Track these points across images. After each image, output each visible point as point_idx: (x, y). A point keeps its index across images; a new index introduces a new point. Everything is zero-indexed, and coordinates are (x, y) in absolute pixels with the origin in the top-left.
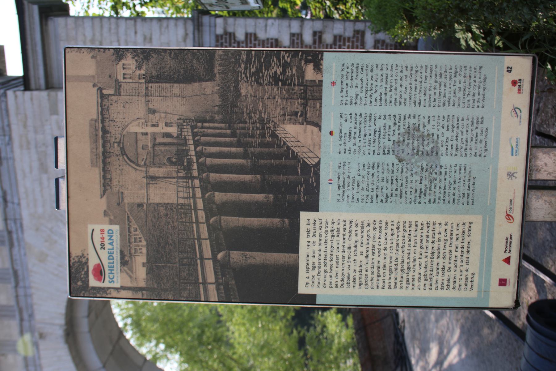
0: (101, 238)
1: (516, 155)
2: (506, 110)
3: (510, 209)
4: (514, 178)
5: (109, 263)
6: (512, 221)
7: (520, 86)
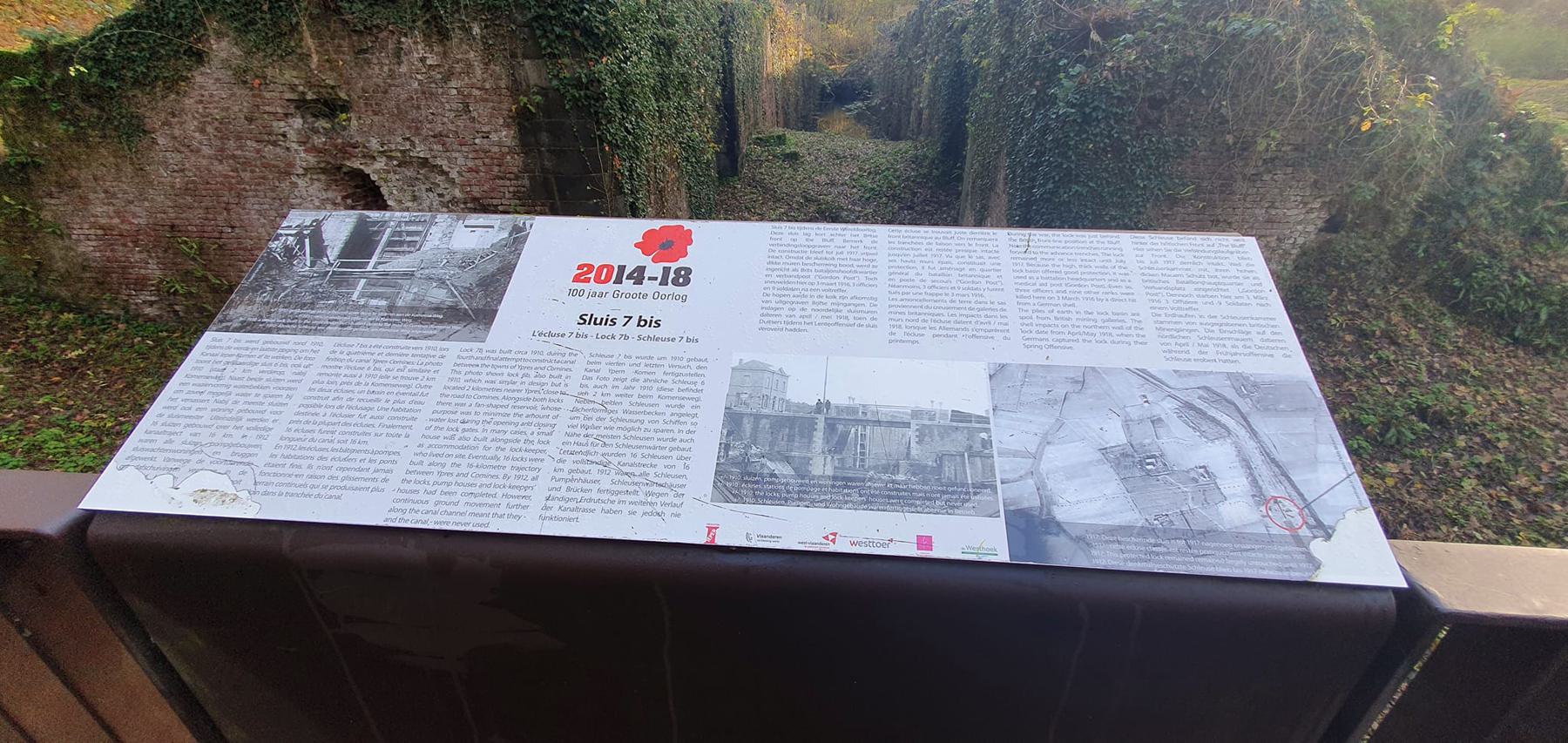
7: (638, 275)
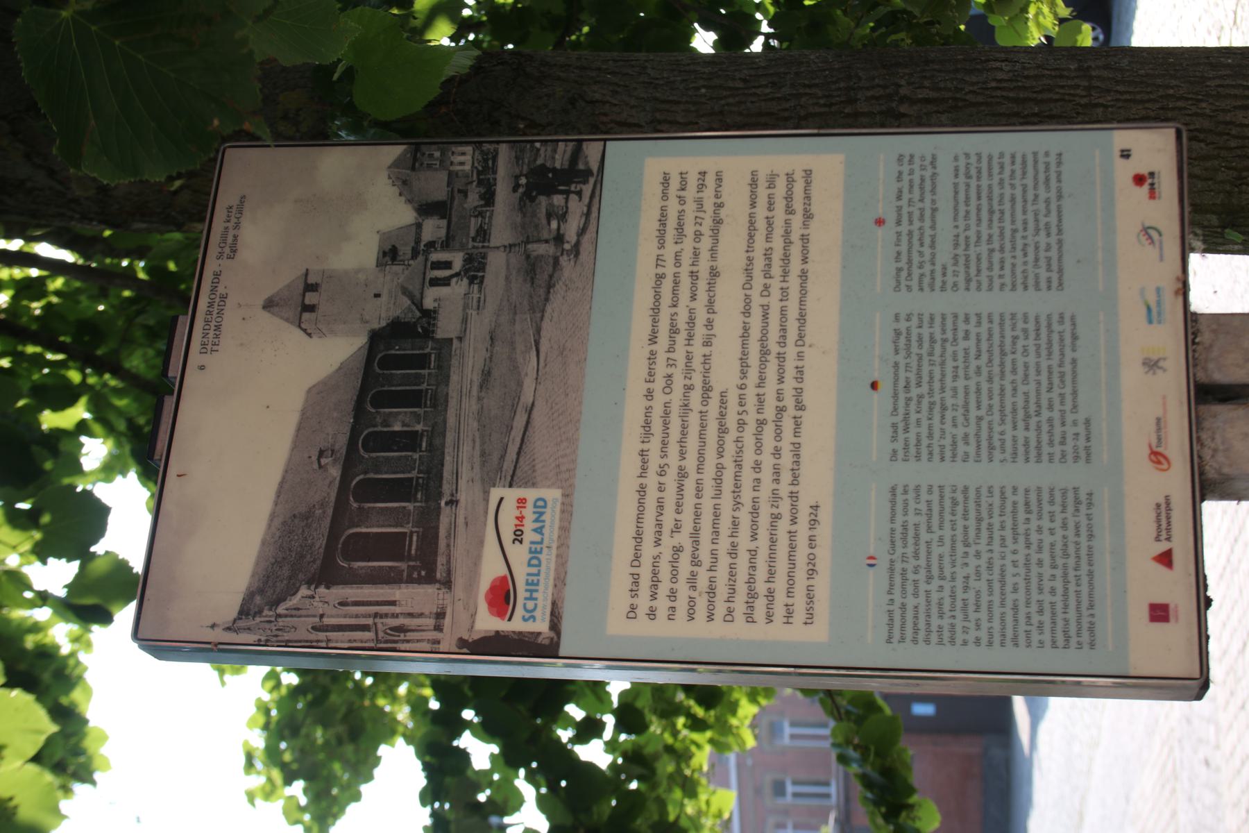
0: (517, 518)
1: (1159, 322)
2: (1126, 231)
3: (1159, 439)
4: (1159, 372)
5: (529, 574)
6: (1165, 466)
7: (1152, 184)
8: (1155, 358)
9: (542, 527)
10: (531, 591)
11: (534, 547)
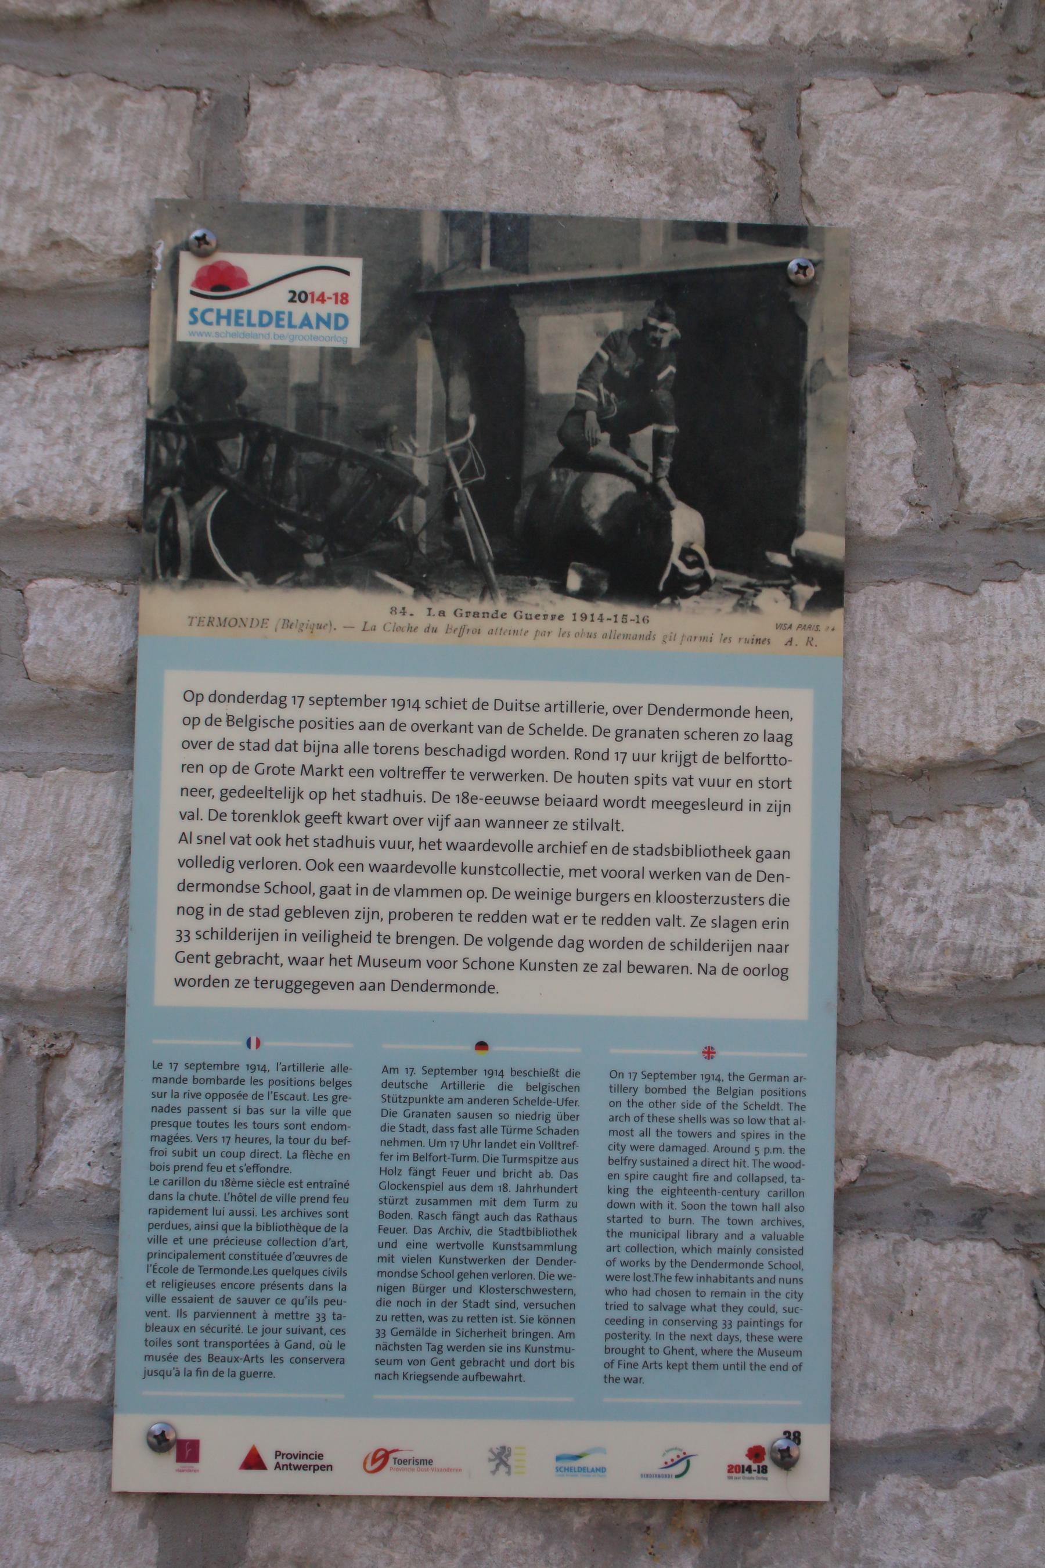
0: (323, 294)
1: (558, 1469)
3: (404, 1462)
4: (493, 1465)
5: (249, 313)
6: (369, 1467)
7: (749, 1469)
8: (511, 1461)
9: (311, 327)
10: (228, 317)
11: (286, 317)
